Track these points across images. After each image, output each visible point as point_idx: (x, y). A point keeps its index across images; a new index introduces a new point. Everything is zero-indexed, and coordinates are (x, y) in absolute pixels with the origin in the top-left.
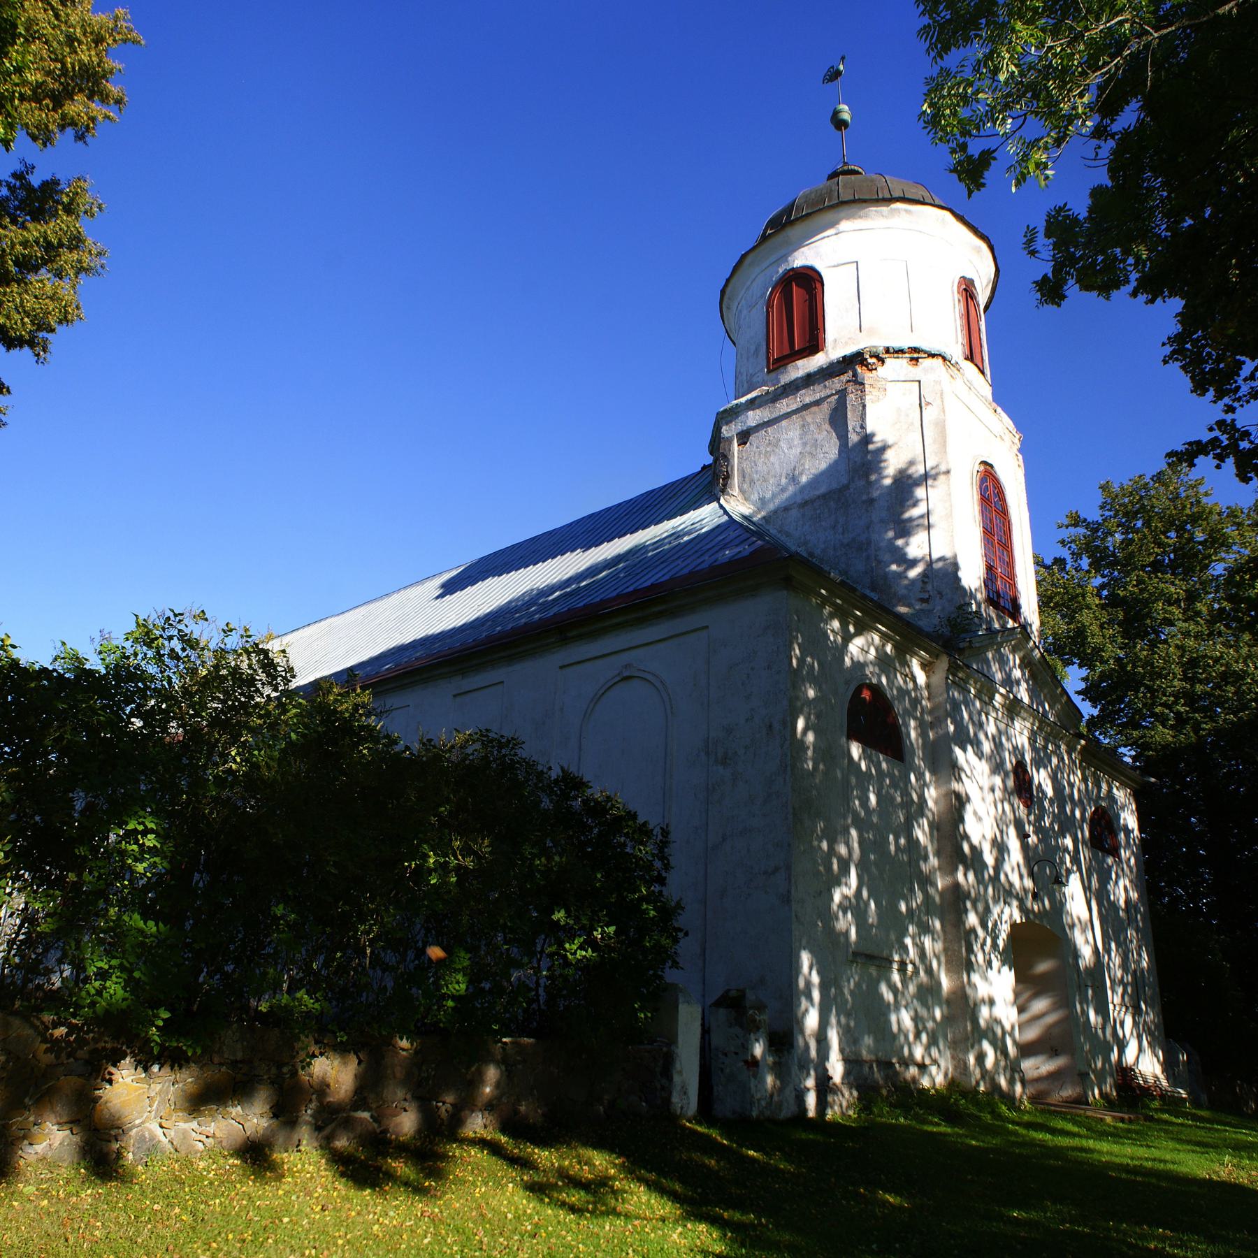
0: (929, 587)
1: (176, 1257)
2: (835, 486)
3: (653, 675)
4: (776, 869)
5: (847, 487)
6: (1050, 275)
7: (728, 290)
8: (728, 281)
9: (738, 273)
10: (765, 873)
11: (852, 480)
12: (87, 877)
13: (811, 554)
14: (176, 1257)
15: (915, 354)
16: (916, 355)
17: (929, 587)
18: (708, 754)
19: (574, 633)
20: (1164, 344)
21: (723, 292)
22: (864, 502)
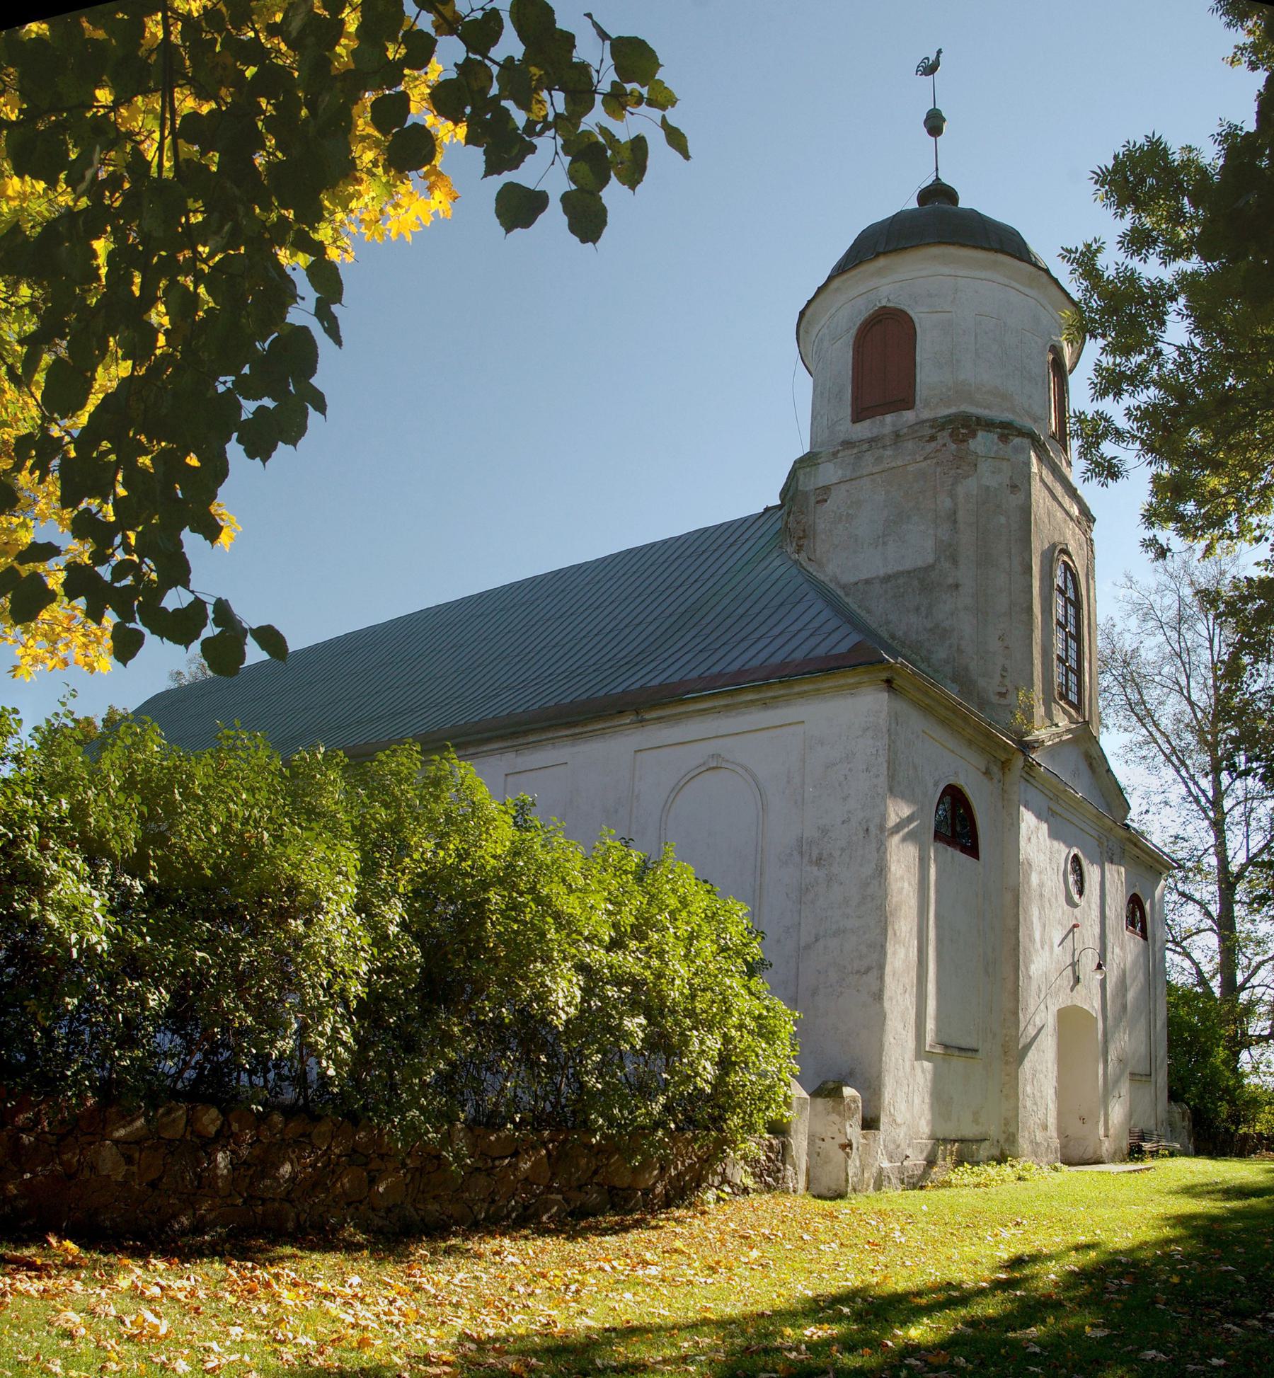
0: (1007, 682)
1: (4, 305)
2: (920, 564)
3: (742, 766)
4: (869, 969)
5: (931, 567)
6: (1166, 470)
7: (808, 313)
8: (809, 302)
9: (822, 297)
10: (858, 972)
11: (937, 560)
12: (184, 1219)
13: (893, 637)
14: (4, 305)
15: (1006, 430)
16: (1006, 432)
17: (1007, 682)
18: (801, 853)
19: (654, 714)
20: (1258, 564)
21: (802, 314)
22: (950, 586)
